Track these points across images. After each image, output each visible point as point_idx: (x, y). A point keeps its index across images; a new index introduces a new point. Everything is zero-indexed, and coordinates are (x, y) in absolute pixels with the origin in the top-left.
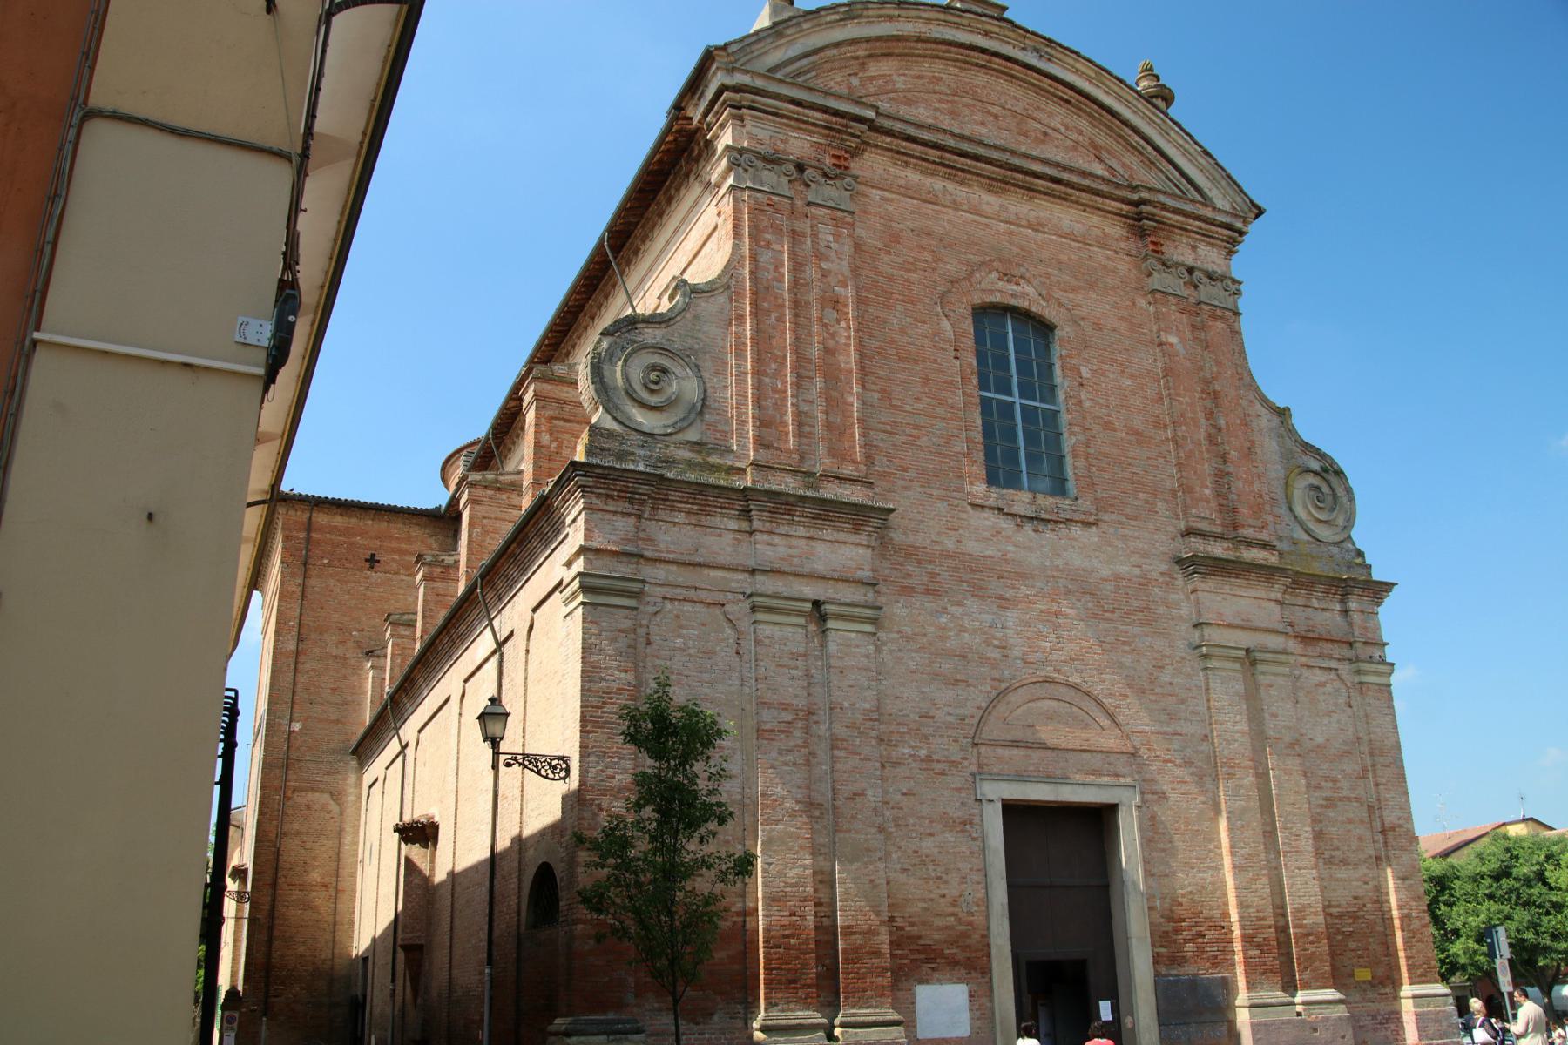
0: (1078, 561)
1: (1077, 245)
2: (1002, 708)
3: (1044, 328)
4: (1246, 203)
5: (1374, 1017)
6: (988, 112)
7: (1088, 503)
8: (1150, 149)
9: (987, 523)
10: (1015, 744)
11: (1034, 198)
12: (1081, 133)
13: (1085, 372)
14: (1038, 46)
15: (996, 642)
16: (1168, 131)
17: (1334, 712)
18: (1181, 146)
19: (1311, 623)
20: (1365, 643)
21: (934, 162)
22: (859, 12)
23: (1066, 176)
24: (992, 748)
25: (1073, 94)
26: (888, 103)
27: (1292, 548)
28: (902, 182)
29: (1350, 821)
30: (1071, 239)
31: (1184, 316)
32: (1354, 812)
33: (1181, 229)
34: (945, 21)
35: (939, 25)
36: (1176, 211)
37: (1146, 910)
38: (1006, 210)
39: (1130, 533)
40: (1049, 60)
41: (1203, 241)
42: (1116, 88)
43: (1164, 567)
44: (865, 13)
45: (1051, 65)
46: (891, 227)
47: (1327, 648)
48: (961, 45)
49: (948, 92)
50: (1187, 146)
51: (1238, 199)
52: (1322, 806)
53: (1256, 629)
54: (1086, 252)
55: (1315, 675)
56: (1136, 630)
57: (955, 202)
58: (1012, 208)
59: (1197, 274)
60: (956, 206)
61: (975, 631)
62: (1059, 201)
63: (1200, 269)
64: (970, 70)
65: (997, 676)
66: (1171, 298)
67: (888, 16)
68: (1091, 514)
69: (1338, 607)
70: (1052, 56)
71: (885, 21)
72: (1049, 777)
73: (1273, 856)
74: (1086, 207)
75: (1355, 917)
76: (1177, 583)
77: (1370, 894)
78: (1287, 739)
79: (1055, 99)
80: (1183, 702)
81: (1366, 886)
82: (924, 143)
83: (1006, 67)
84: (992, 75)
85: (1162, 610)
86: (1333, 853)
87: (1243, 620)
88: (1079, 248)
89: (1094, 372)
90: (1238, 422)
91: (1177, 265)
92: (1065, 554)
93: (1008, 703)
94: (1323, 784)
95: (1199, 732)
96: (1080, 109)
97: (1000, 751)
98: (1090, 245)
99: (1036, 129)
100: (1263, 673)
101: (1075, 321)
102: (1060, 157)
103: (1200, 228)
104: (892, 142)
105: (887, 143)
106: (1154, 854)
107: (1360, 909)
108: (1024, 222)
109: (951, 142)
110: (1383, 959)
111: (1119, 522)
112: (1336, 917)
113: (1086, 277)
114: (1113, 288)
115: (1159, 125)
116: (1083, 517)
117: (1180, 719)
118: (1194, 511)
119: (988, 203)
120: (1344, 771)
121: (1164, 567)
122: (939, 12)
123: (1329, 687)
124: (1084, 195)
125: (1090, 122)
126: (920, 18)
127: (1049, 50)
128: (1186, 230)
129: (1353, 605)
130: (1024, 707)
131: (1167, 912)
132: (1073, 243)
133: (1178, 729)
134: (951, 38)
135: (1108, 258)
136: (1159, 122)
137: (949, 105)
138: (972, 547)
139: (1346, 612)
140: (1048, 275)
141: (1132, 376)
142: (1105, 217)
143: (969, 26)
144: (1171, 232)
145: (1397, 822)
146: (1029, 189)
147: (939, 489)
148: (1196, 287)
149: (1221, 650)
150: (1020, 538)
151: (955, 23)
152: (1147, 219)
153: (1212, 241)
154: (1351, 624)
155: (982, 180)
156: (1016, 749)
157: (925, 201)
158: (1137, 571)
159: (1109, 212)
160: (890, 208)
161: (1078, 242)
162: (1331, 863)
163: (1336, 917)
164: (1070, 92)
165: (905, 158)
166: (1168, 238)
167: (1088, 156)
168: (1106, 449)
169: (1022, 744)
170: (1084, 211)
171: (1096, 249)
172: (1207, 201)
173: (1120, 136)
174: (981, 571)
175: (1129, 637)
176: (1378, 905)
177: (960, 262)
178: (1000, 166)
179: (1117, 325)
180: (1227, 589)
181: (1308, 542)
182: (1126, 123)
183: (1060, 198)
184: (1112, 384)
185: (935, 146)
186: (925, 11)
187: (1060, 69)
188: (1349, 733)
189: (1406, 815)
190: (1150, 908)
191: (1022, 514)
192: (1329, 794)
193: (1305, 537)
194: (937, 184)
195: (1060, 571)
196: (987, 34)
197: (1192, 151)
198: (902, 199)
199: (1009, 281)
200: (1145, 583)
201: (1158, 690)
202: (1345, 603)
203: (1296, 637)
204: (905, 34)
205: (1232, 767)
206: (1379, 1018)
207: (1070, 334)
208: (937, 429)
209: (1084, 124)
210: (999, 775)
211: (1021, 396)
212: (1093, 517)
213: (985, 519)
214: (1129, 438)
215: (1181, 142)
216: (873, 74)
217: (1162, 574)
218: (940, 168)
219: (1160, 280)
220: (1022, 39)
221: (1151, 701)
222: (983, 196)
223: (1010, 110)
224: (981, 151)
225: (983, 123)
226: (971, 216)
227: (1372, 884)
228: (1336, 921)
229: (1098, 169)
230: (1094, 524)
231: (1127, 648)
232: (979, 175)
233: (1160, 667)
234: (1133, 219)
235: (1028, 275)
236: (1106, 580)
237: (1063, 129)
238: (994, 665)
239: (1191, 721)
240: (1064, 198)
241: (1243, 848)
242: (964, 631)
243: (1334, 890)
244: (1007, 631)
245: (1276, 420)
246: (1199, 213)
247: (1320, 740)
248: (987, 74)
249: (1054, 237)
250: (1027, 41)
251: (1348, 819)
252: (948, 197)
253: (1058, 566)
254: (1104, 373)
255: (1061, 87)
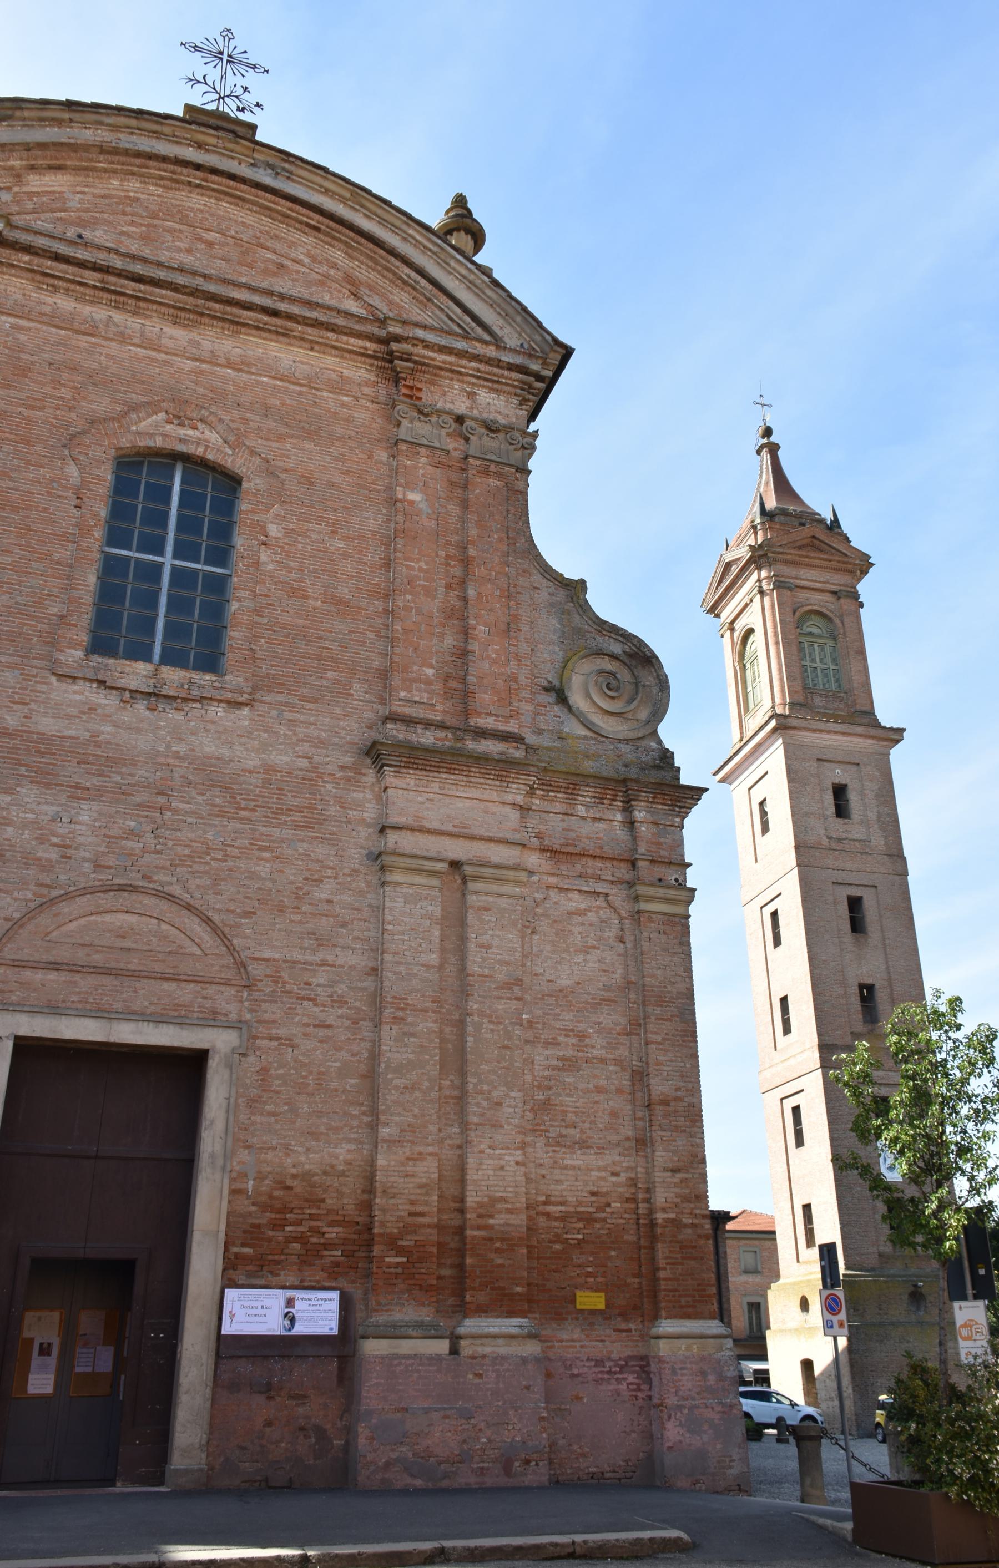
0: (209, 747)
1: (298, 388)
2: (44, 920)
3: (231, 482)
4: (546, 341)
5: (599, 1362)
6: (200, 239)
7: (241, 679)
8: (423, 282)
9: (78, 697)
10: (55, 966)
11: (239, 333)
12: (334, 266)
13: (273, 530)
14: (271, 161)
15: (55, 840)
16: (448, 260)
17: (594, 947)
18: (463, 276)
19: (573, 835)
20: (652, 861)
21: (95, 287)
22: (9, 112)
23: (283, 306)
24: (17, 969)
25: (321, 218)
26: (52, 223)
27: (557, 744)
28: (47, 309)
29: (599, 1090)
30: (290, 382)
31: (438, 470)
32: (608, 1078)
33: (452, 371)
34: (139, 129)
35: (132, 133)
36: (443, 349)
37: (226, 1192)
38: (197, 345)
39: (302, 718)
40: (288, 178)
41: (483, 386)
42: (379, 211)
43: (348, 760)
44: (18, 113)
45: (291, 183)
46: (19, 358)
47: (593, 866)
48: (164, 159)
49: (144, 214)
50: (472, 277)
51: (537, 338)
52: (555, 1068)
53: (473, 838)
54: (310, 397)
55: (570, 900)
56: (288, 833)
57: (122, 334)
58: (207, 345)
59: (469, 423)
60: (123, 338)
61: (25, 825)
62: (274, 337)
63: (472, 419)
64: (179, 190)
65: (48, 881)
66: (423, 451)
67: (53, 119)
68: (242, 693)
69: (619, 817)
70: (291, 173)
71: (50, 126)
72: (100, 1010)
73: (457, 1130)
74: (312, 345)
75: (588, 1219)
76: (364, 779)
77: (620, 1190)
78: (501, 977)
79: (297, 225)
80: (344, 925)
81: (614, 1179)
82: (82, 264)
83: (229, 187)
84: (210, 197)
85: (333, 810)
86: (564, 1131)
87: (454, 826)
88: (300, 393)
89: (288, 531)
90: (498, 593)
91: (440, 412)
92: (193, 738)
93: (56, 915)
94: (561, 1039)
95: (363, 963)
96: (334, 238)
97: (28, 973)
98: (317, 389)
99: (269, 260)
100: (475, 892)
101: (269, 470)
102: (298, 291)
103: (478, 370)
104: (30, 260)
105: (25, 263)
106: (258, 1119)
107: (601, 1209)
108: (222, 361)
109: (118, 263)
110: (630, 1280)
111: (287, 704)
112: (556, 1219)
113: (303, 424)
114: (341, 438)
115: (435, 253)
116: (229, 695)
117: (334, 946)
118: (402, 694)
119: (171, 338)
120: (600, 1023)
121: (348, 760)
122: (130, 117)
123: (592, 916)
124: (309, 330)
125: (346, 253)
126: (101, 123)
127: (287, 166)
128: (459, 373)
129: (639, 815)
130: (83, 921)
131: (263, 1199)
132: (292, 387)
133: (330, 958)
134: (148, 150)
135: (343, 405)
136: (435, 249)
137: (144, 228)
138: (47, 724)
139: (631, 824)
140: (245, 421)
141: (348, 538)
142: (342, 357)
143: (174, 136)
144: (435, 375)
145: (674, 1094)
146: (232, 322)
147: (10, 655)
148: (467, 440)
149: (408, 860)
150: (126, 717)
151: (154, 132)
152: (401, 359)
153: (496, 386)
154: (635, 839)
155: (163, 309)
156: (56, 973)
157: (77, 332)
158: (304, 763)
159: (350, 352)
160: (23, 338)
161: (302, 385)
162: (558, 1144)
163: (556, 1219)
164: (317, 217)
165: (51, 281)
166: (432, 383)
167: (340, 291)
168: (287, 619)
169: (65, 967)
170: (312, 349)
171: (325, 394)
172: (497, 342)
173: (388, 270)
174: (54, 754)
175: (273, 842)
176: (633, 1206)
177: (114, 401)
178: (191, 294)
179: (338, 478)
180: (435, 787)
181: (585, 737)
182: (392, 252)
183: (277, 333)
184: (314, 546)
185: (96, 268)
186: (108, 115)
187: (304, 189)
188: (617, 976)
189: (690, 1086)
190: (234, 1192)
191: (132, 688)
192: (570, 1053)
193: (583, 732)
194: (100, 313)
195: (179, 758)
196: (200, 146)
197: (478, 282)
198: (44, 328)
199: (181, 425)
200: (313, 776)
201: (304, 908)
202: (631, 812)
203: (543, 850)
204: (79, 142)
205: (402, 1009)
206: (608, 1364)
207: (259, 487)
208: (26, 587)
209: (337, 255)
210: (19, 1004)
211: (176, 556)
212: (246, 696)
213: (75, 692)
214: (325, 607)
215: (464, 272)
216: (35, 189)
217: (342, 768)
218: (101, 294)
219: (412, 427)
220: (249, 153)
221: (291, 921)
222: (165, 329)
223: (232, 237)
224: (162, 274)
225: (189, 251)
226: (144, 351)
227: (623, 1178)
228: (557, 1224)
229: (352, 306)
230: (247, 705)
231: (266, 855)
232: (160, 304)
233: (316, 880)
234: (383, 359)
235: (211, 418)
236: (250, 772)
237: (307, 260)
238: (46, 867)
239: (353, 949)
240: (284, 334)
241: (400, 1115)
242: (8, 825)
243: (558, 1182)
244: (78, 827)
245: (561, 595)
246: (476, 352)
247: (565, 982)
248: (202, 195)
249: (265, 379)
250: (255, 155)
251: (596, 1087)
252: (113, 328)
253: (178, 752)
254: (304, 534)
255: (304, 211)
